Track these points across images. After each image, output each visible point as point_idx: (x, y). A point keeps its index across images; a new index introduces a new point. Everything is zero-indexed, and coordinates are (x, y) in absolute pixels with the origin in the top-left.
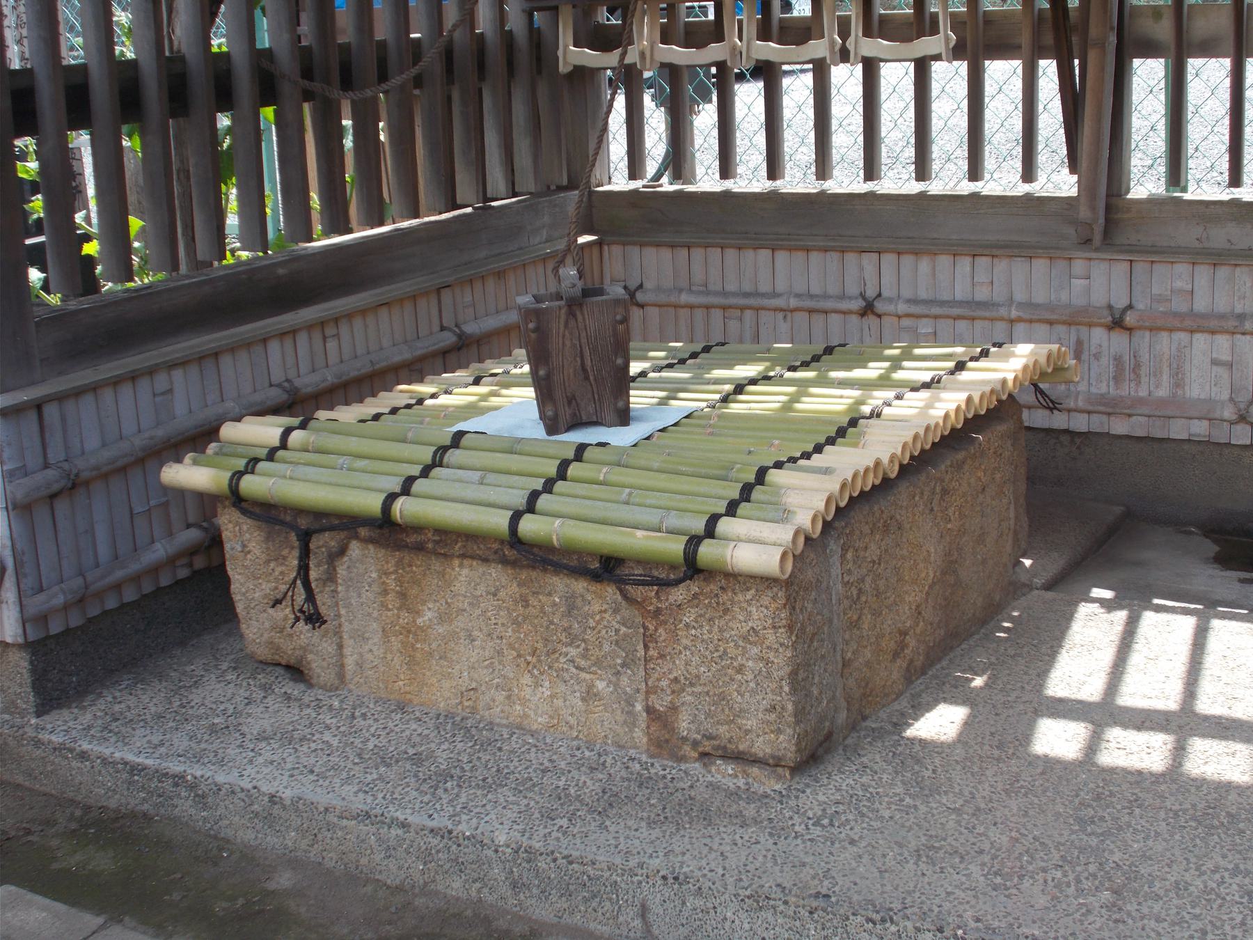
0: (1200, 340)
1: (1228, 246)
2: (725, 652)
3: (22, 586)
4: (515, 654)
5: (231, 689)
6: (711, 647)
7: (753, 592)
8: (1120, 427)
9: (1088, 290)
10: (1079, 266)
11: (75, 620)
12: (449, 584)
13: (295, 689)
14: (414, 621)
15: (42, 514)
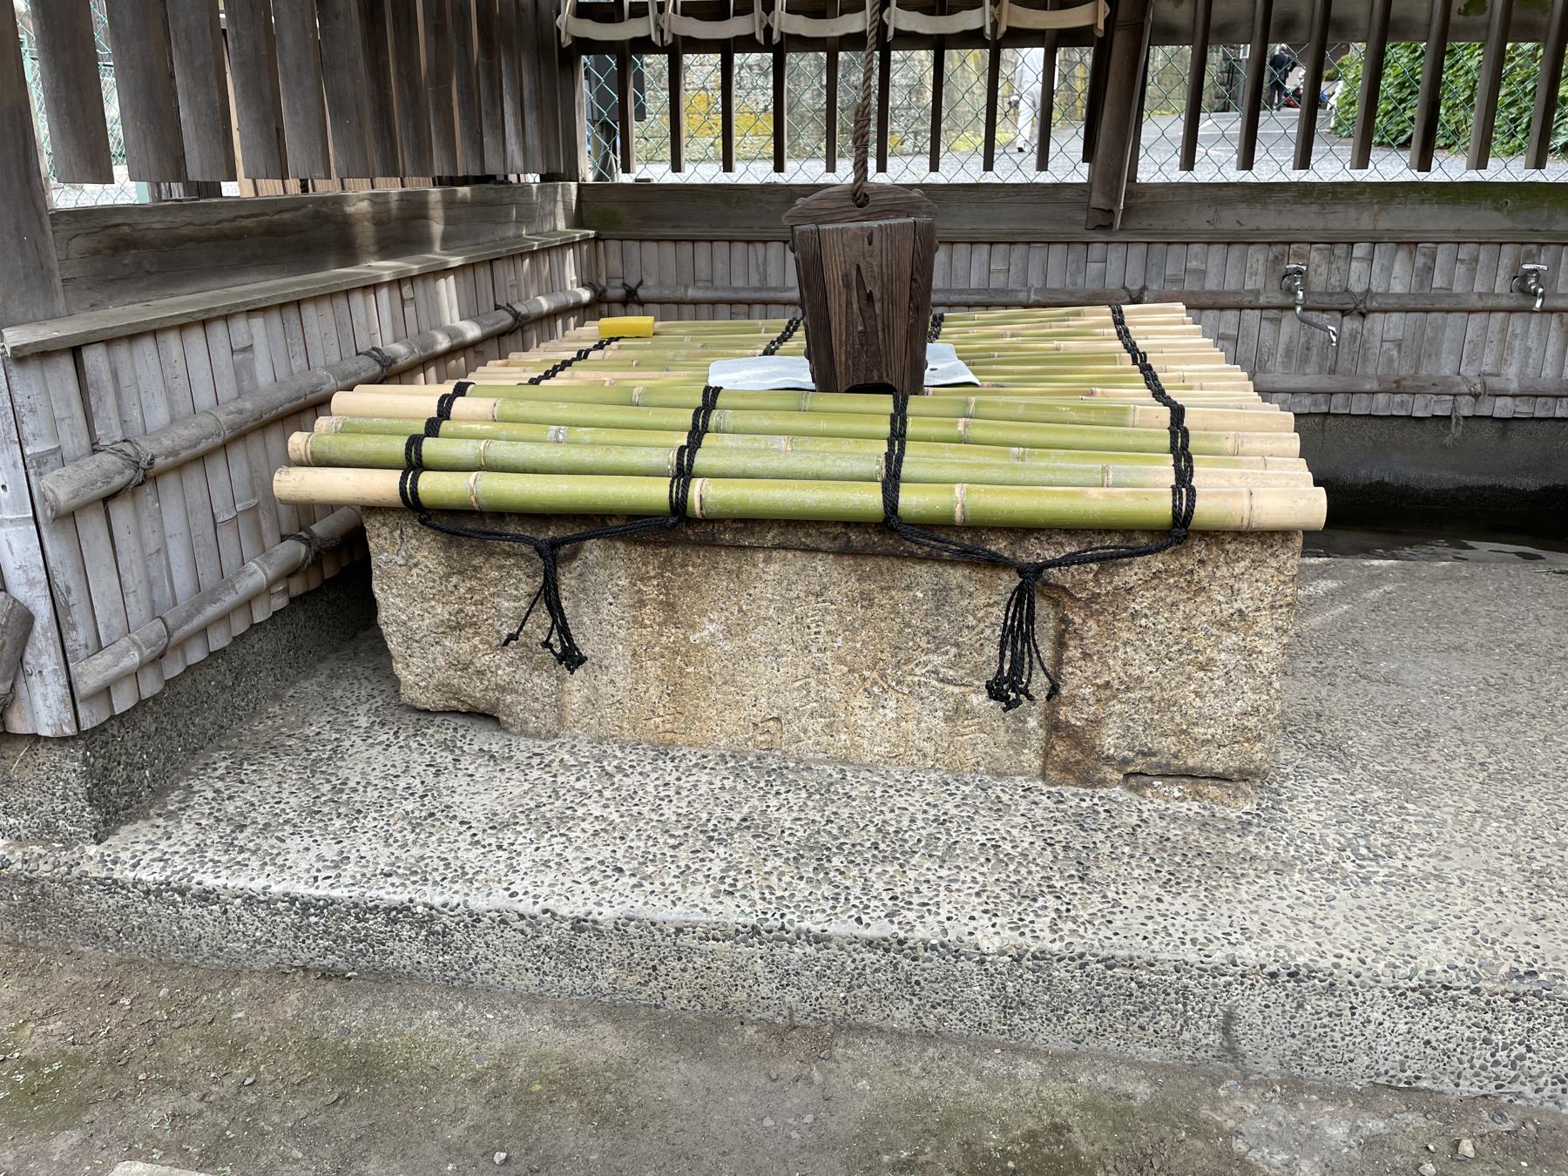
1: (1238, 227)
2: (1189, 644)
3: (68, 644)
4: (845, 669)
6: (1169, 639)
7: (1247, 562)
10: (1096, 251)
13: (494, 742)
14: (686, 638)
15: (93, 527)
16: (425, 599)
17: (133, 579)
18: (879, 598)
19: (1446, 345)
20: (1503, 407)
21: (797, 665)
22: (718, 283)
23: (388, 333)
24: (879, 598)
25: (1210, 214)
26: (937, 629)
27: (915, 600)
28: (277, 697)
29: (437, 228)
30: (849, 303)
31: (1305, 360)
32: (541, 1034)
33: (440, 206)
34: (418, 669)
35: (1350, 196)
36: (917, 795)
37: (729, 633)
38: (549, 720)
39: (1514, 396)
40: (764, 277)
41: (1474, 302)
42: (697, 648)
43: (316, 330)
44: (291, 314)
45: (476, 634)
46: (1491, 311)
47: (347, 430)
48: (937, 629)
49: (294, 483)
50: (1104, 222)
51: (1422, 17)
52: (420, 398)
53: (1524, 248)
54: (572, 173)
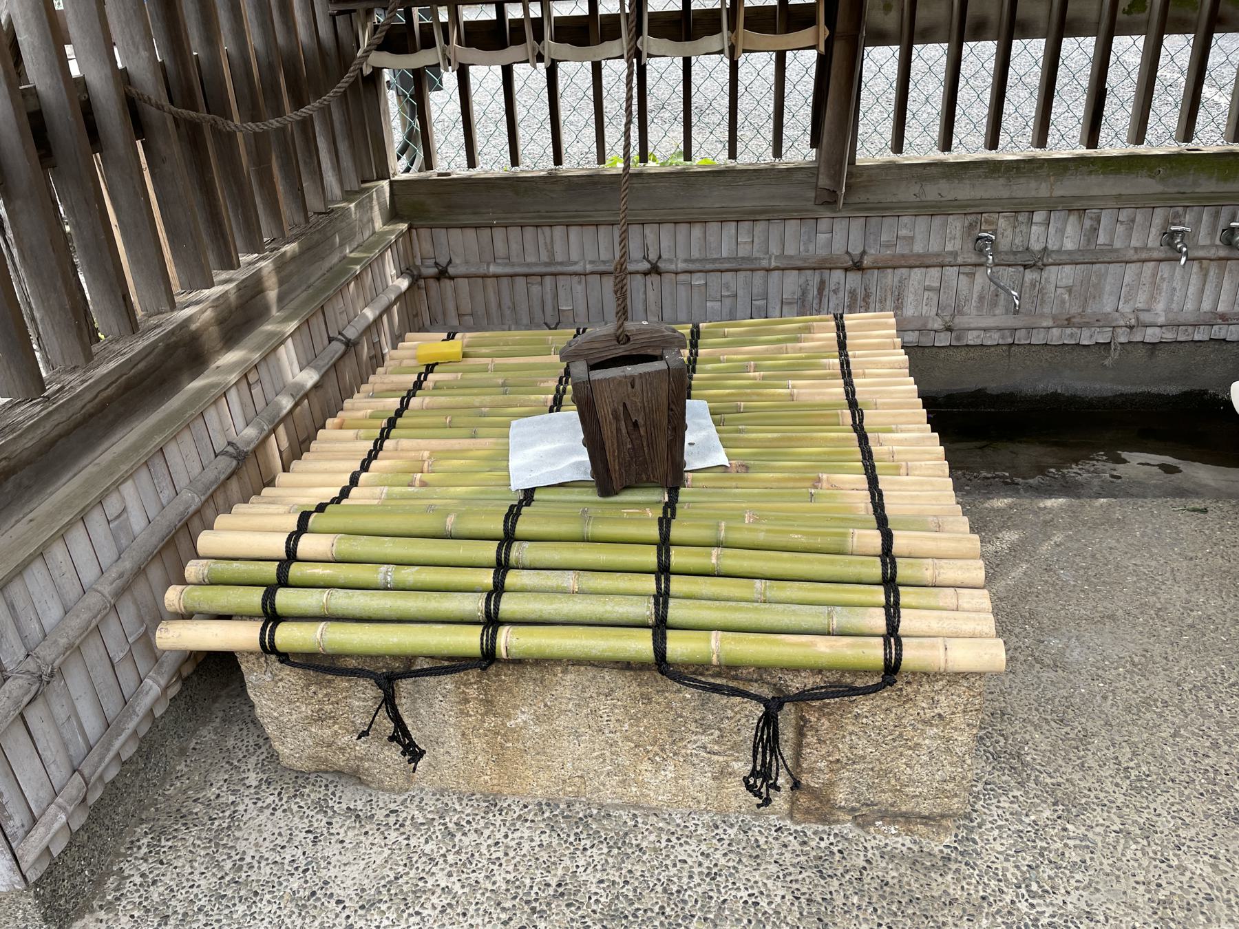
0: (917, 273)
1: (939, 198)
2: (901, 735)
10: (824, 224)
16: (291, 702)
18: (655, 698)
19: (1108, 288)
20: (1152, 335)
21: (594, 742)
22: (514, 259)
24: (655, 698)
25: (916, 189)
26: (703, 719)
27: (684, 698)
28: (183, 752)
30: (618, 430)
31: (994, 304)
33: (273, 274)
35: (1031, 171)
36: (693, 842)
37: (538, 720)
39: (1161, 326)
41: (1131, 255)
42: (513, 730)
43: (178, 460)
45: (335, 723)
46: (1144, 261)
48: (703, 719)
50: (829, 200)
51: (1092, 15)
53: (1172, 210)
54: (384, 174)
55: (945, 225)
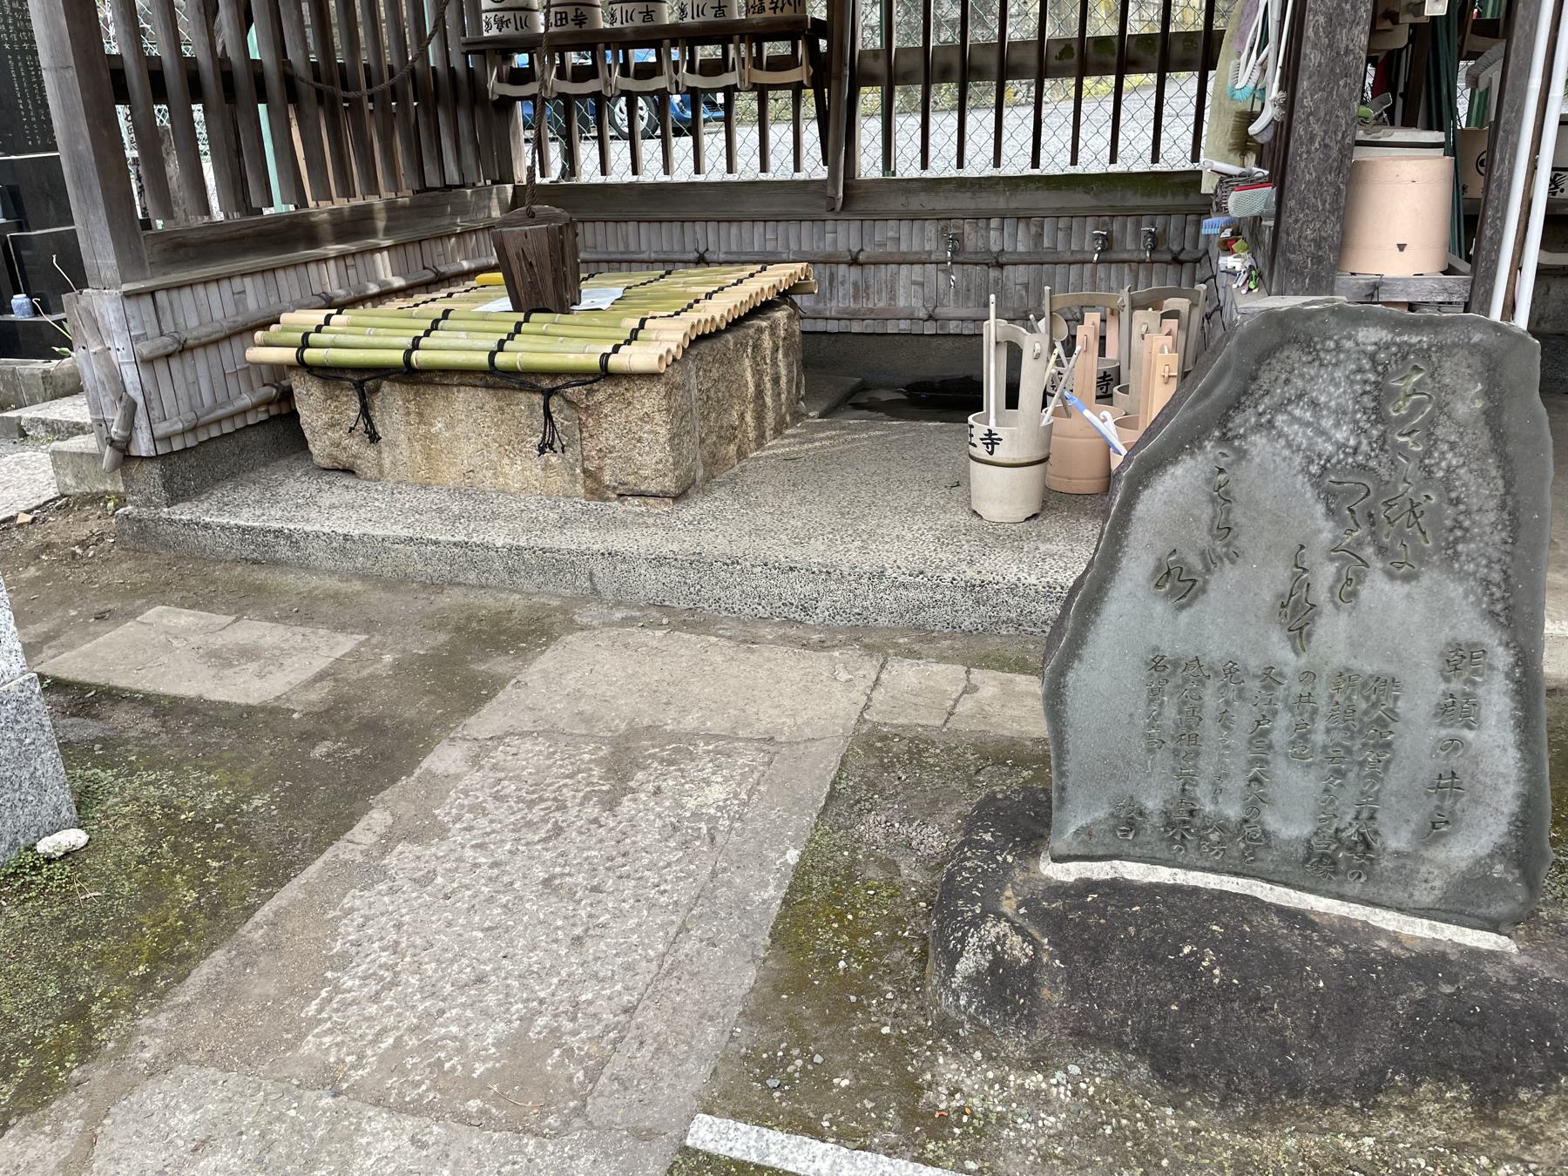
5: (305, 486)
8: (856, 327)
9: (835, 241)
10: (829, 225)
11: (191, 442)
12: (451, 404)
17: (181, 392)
23: (335, 283)
25: (902, 199)
29: (381, 224)
32: (332, 583)
34: (318, 447)
37: (447, 428)
38: (374, 472)
40: (627, 244)
41: (1068, 257)
44: (269, 276)
47: (284, 330)
49: (256, 354)
52: (319, 316)
55: (923, 229)
